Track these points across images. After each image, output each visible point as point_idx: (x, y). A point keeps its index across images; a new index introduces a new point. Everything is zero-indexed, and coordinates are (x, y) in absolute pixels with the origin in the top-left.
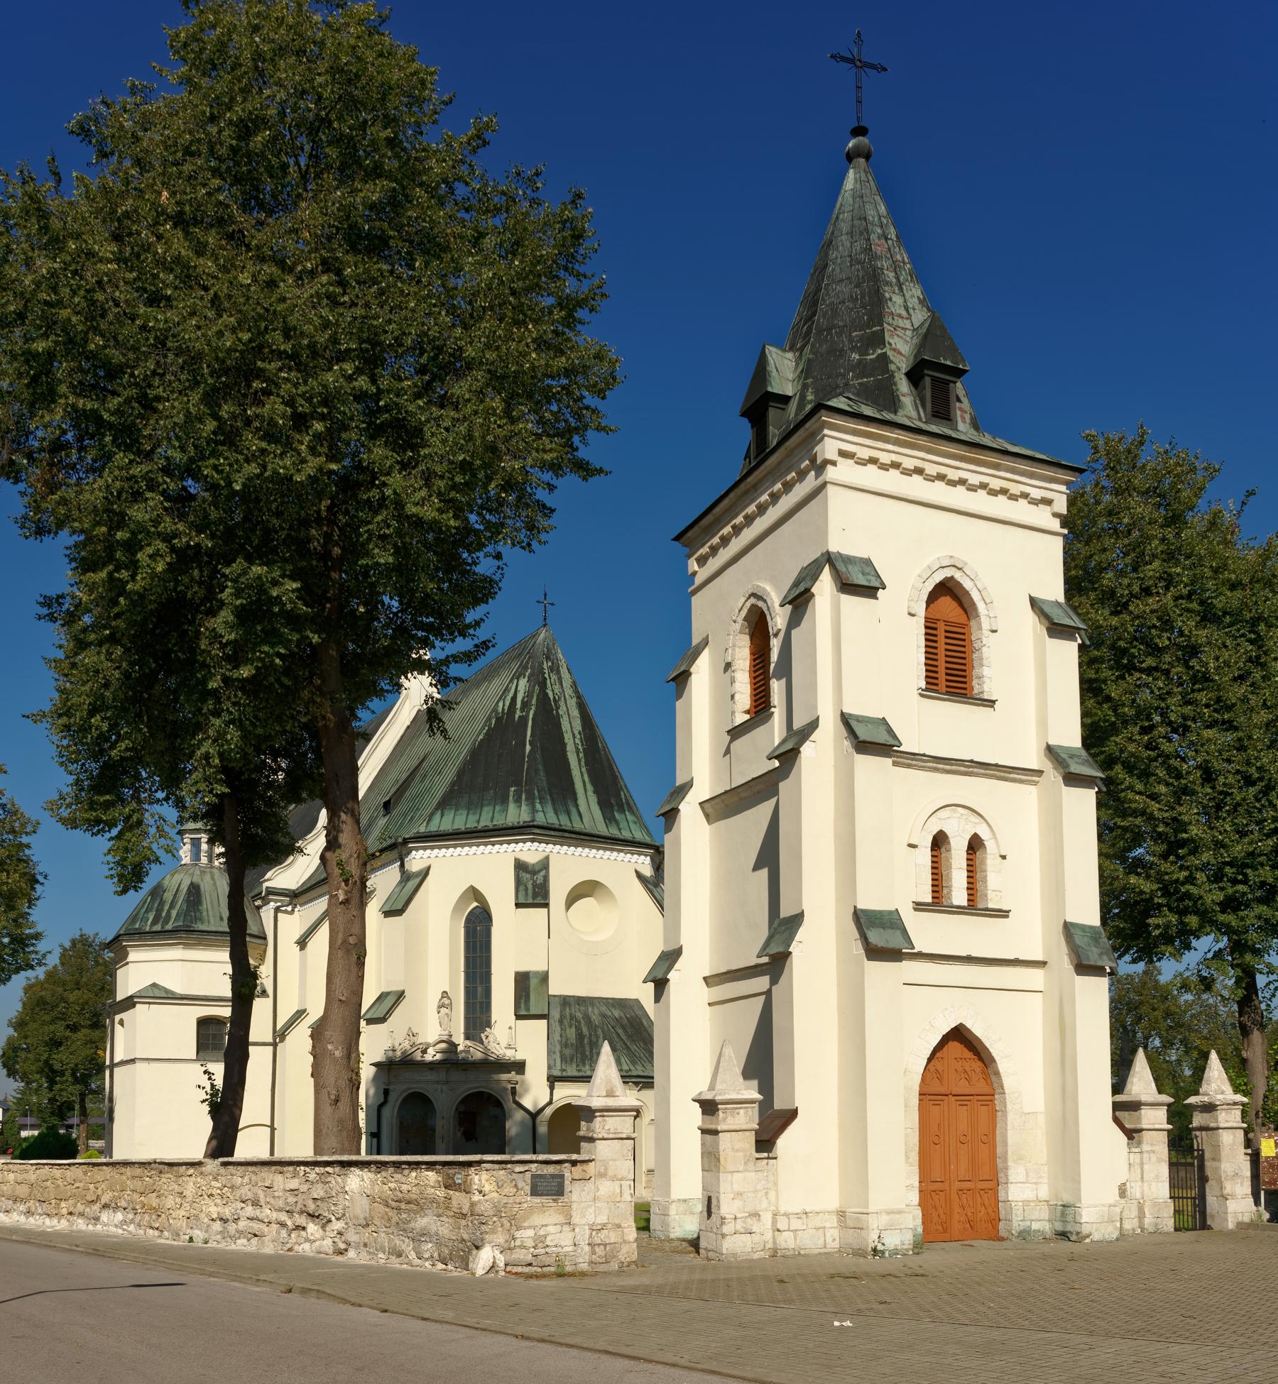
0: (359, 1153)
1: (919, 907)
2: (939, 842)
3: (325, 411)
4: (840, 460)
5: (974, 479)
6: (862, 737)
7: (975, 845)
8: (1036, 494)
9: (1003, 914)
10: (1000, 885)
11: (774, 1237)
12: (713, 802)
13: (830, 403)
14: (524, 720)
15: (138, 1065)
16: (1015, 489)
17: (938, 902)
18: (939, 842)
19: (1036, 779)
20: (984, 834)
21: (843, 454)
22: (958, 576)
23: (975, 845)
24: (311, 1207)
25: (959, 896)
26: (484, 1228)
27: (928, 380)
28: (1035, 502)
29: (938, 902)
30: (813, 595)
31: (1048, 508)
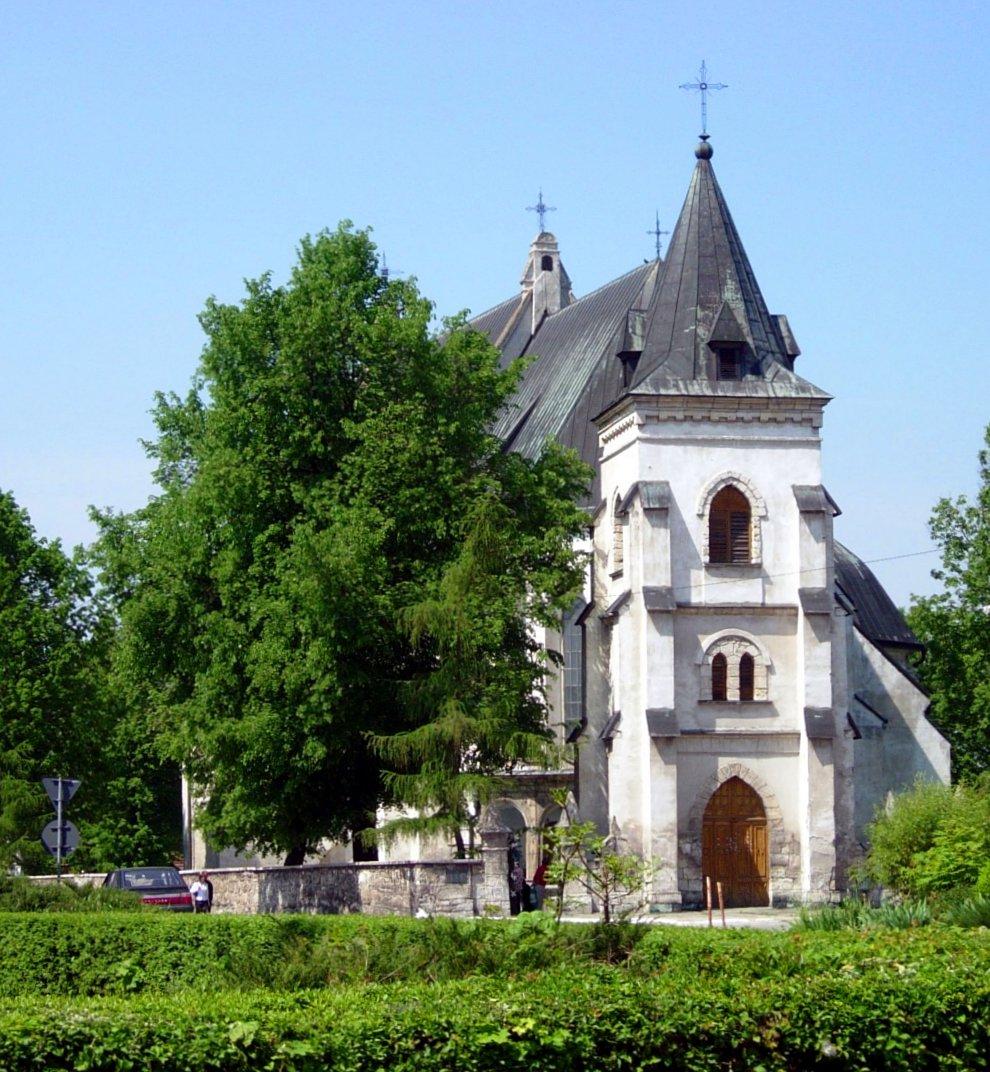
7: (747, 663)
13: (634, 392)
20: (752, 651)
22: (735, 483)
23: (747, 663)
25: (733, 694)
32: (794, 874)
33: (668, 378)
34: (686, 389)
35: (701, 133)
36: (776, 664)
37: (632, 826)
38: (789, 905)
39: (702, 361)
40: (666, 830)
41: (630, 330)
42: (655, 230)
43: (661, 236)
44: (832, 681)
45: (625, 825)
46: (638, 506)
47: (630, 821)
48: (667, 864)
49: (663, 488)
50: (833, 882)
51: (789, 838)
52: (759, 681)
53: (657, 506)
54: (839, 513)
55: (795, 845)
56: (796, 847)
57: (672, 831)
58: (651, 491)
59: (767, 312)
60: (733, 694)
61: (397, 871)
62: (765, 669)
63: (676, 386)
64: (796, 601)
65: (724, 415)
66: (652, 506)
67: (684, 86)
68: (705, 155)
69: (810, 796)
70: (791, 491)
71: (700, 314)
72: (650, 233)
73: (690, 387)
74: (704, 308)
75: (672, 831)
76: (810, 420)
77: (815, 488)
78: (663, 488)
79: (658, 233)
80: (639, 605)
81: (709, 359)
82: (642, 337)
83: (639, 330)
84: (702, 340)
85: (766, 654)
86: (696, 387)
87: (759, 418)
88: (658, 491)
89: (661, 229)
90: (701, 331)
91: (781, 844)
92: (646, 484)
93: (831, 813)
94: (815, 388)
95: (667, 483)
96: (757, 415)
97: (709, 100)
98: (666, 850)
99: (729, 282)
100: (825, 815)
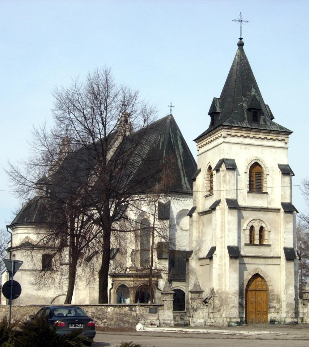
0: (108, 303)
2: (252, 228)
5: (263, 137)
7: (262, 229)
8: (280, 138)
9: (269, 245)
10: (269, 238)
13: (223, 124)
14: (162, 150)
15: (18, 234)
16: (274, 138)
17: (251, 243)
18: (252, 228)
19: (278, 211)
20: (264, 225)
21: (228, 134)
22: (258, 161)
23: (262, 229)
24: (98, 316)
25: (257, 242)
26: (139, 320)
28: (281, 141)
29: (251, 243)
31: (284, 141)
32: (278, 311)
33: (234, 121)
34: (241, 125)
35: (240, 37)
36: (272, 230)
37: (220, 292)
38: (276, 323)
39: (246, 116)
40: (235, 293)
41: (215, 105)
42: (170, 105)
43: (172, 107)
44: (293, 238)
45: (217, 291)
46: (223, 166)
47: (219, 289)
48: (236, 307)
49: (233, 161)
50: (294, 314)
51: (276, 297)
52: (266, 237)
53: (232, 168)
54: (294, 175)
55: (279, 301)
56: (278, 300)
57: (237, 293)
58: (229, 162)
59: (264, 104)
60: (257, 242)
61: (127, 308)
62: (268, 232)
63: (238, 123)
64: (280, 207)
65: (254, 136)
66: (230, 168)
67: (234, 20)
68: (241, 45)
69: (286, 281)
70: (278, 165)
71: (244, 99)
72: (169, 106)
73: (242, 124)
74: (245, 97)
75: (237, 293)
76: (284, 140)
77: (286, 165)
78: (233, 161)
79: (171, 106)
80: (224, 205)
81: (248, 115)
82: (220, 108)
83: (218, 105)
84: (245, 108)
85: (269, 227)
86: (245, 124)
87: (266, 138)
88: (231, 162)
89: (170, 107)
90: (244, 105)
91: (273, 299)
92: (226, 159)
93: (293, 288)
94: (286, 129)
95: (234, 160)
96: (266, 136)
97: (242, 26)
98: (235, 301)
99: (253, 89)
100: (291, 288)
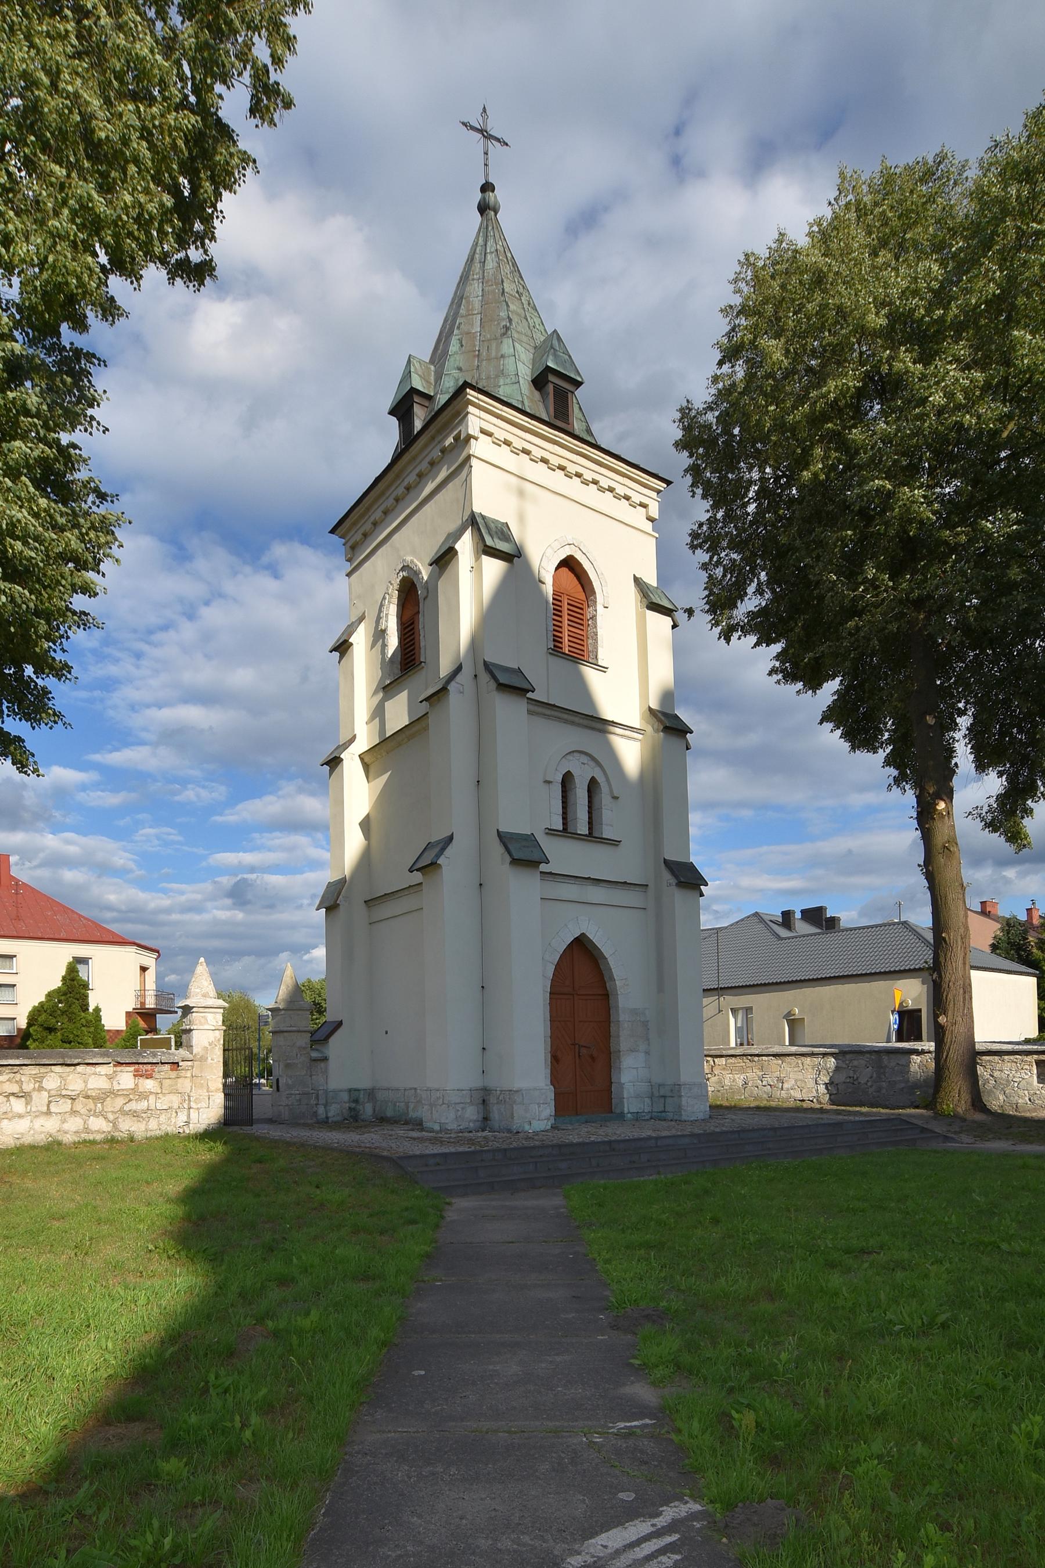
1: (551, 832)
2: (567, 780)
3: (423, 1373)
4: (482, 436)
6: (489, 542)
7: (593, 786)
9: (615, 843)
11: (206, 252)
12: (377, 749)
18: (567, 780)
20: (601, 779)
21: (483, 431)
22: (579, 556)
23: (593, 786)
25: (583, 829)
27: (551, 387)
29: (566, 831)
30: (456, 552)
